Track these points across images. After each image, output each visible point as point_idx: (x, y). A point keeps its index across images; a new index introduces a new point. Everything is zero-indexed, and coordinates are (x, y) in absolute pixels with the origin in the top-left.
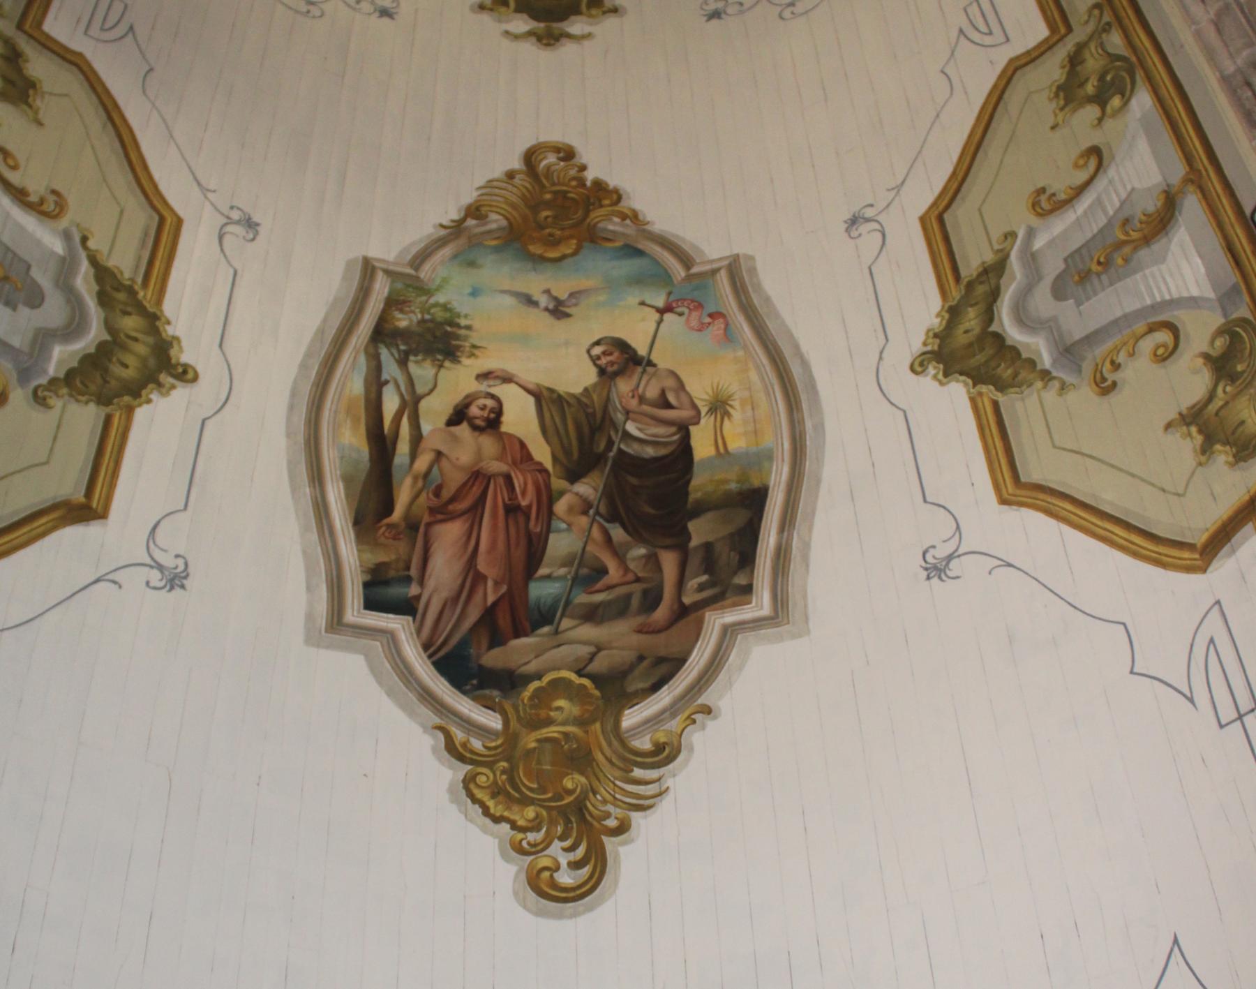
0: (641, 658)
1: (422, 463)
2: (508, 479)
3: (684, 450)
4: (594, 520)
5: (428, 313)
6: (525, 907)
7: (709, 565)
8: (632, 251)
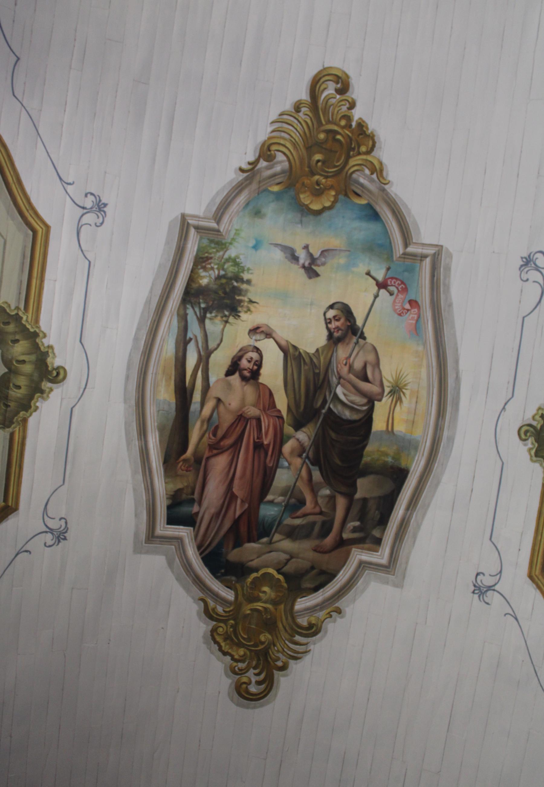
0: (313, 568)
1: (207, 411)
2: (259, 420)
3: (368, 420)
4: (304, 462)
5: (223, 269)
6: (232, 700)
7: (362, 517)
8: (373, 215)
